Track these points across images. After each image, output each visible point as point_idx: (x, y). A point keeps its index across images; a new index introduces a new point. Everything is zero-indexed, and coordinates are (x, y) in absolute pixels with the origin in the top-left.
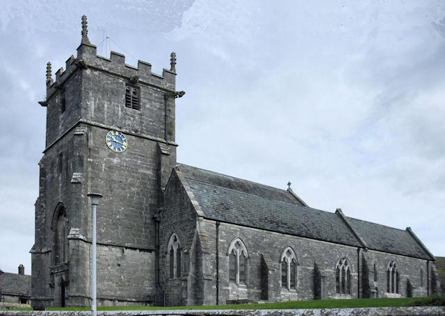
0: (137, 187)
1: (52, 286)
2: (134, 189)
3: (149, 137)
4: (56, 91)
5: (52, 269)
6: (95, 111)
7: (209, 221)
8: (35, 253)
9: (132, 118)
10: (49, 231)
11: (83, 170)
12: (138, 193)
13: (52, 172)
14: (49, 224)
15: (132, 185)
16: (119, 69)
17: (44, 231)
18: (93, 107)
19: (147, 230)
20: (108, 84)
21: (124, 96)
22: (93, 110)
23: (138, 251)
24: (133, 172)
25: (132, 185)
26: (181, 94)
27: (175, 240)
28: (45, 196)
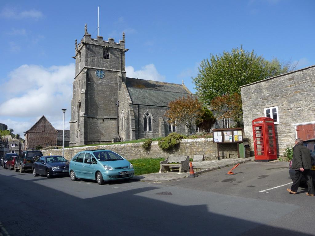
0: (109, 92)
1: (77, 137)
2: (108, 93)
3: (114, 70)
4: (78, 53)
5: (77, 129)
6: (91, 62)
7: (134, 105)
8: (71, 123)
9: (106, 63)
10: (76, 113)
11: (239, 154)
12: (109, 95)
13: (77, 87)
14: (76, 110)
15: (106, 91)
16: (100, 43)
17: (75, 112)
18: (90, 60)
19: (114, 110)
20: (96, 50)
21: (103, 54)
22: (90, 61)
23: (110, 119)
24: (107, 86)
25: (106, 91)
26: (127, 50)
27: (123, 114)
28: (75, 98)
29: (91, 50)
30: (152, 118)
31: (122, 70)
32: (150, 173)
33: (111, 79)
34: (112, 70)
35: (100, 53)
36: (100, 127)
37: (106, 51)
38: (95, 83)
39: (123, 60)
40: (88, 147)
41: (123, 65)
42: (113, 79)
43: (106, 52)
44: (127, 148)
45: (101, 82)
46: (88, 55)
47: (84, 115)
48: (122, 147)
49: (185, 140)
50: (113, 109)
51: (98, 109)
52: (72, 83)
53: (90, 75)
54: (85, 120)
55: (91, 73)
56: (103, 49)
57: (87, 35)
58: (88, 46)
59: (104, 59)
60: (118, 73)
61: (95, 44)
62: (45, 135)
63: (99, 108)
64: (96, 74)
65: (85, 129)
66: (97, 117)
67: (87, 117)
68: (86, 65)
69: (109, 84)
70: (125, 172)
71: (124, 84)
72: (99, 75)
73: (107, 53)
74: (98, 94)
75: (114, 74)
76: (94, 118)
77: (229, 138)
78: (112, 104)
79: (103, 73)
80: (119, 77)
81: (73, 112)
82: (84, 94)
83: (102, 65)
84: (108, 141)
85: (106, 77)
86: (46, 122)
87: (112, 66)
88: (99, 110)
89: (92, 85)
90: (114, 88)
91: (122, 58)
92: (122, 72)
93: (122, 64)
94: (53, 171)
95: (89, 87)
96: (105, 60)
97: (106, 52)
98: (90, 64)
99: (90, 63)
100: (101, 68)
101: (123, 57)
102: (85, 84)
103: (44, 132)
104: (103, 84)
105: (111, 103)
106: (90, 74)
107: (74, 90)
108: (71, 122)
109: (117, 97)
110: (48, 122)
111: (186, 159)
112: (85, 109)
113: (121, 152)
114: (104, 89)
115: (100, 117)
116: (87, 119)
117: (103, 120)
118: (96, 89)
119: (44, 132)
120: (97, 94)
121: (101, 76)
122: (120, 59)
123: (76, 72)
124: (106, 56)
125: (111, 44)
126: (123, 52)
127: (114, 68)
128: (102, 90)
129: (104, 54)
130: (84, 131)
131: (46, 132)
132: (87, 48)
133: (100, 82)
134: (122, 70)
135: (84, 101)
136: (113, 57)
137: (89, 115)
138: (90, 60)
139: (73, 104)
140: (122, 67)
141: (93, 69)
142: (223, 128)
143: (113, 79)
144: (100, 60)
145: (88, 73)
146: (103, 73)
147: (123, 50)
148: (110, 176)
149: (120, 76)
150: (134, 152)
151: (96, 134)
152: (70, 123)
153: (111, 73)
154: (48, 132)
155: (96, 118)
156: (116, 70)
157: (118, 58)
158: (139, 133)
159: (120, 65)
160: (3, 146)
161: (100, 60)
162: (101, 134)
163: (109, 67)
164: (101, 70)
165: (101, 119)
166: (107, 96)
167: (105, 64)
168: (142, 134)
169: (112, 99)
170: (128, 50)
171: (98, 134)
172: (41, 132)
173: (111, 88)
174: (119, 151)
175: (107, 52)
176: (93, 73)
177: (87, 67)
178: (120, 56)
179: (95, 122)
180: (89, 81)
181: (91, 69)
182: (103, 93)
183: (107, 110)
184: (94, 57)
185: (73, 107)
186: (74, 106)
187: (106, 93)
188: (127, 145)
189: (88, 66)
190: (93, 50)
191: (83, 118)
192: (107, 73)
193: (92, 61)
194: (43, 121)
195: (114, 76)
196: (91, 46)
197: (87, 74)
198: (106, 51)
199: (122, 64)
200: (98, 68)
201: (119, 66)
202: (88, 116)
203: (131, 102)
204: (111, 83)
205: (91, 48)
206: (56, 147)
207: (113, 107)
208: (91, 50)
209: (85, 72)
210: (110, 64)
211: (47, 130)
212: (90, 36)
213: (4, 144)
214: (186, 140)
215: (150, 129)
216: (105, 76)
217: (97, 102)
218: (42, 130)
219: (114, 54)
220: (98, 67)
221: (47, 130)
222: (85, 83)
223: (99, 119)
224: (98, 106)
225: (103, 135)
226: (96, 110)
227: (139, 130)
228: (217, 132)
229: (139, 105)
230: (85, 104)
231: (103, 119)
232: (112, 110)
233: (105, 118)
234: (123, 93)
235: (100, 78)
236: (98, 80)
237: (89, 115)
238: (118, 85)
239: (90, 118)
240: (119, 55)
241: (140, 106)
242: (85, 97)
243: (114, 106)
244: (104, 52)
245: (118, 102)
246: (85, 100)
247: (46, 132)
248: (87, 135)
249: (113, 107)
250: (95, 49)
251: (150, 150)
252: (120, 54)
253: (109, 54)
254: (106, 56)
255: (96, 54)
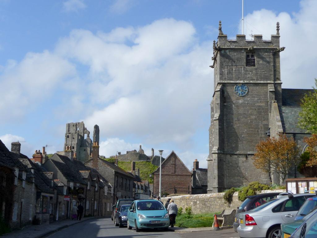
2: (253, 117)
3: (262, 82)
6: (227, 74)
9: (250, 73)
12: (255, 119)
15: (252, 114)
16: (242, 45)
18: (226, 72)
20: (234, 55)
21: (245, 60)
22: (226, 73)
26: (283, 49)
29: (228, 57)
31: (275, 80)
32: (205, 227)
33: (259, 95)
34: (259, 82)
35: (240, 59)
36: (242, 168)
37: (250, 54)
38: (234, 104)
39: (277, 65)
40: (182, 197)
41: (277, 73)
42: (261, 95)
43: (250, 57)
44: (212, 199)
45: (243, 101)
46: (223, 65)
47: (218, 150)
48: (208, 197)
49: (264, 191)
51: (238, 141)
52: (210, 103)
53: (226, 93)
54: (218, 157)
55: (228, 90)
56: (245, 54)
57: (222, 37)
58: (223, 52)
59: (246, 67)
60: (269, 86)
61: (233, 47)
62: (175, 179)
63: (241, 139)
64: (235, 90)
65: (218, 171)
66: (238, 152)
67: (222, 153)
68: (221, 79)
69: (255, 104)
70: (157, 222)
71: (274, 102)
72: (240, 92)
73: (251, 57)
74: (238, 120)
75: (263, 87)
76: (232, 154)
77: (304, 190)
78: (260, 132)
79: (246, 88)
80: (270, 91)
81: (211, 145)
82: (217, 121)
83: (244, 77)
85: (250, 93)
86: (177, 161)
87: (259, 76)
88: (240, 143)
89: (230, 107)
90: (263, 109)
91: (275, 62)
92: (275, 84)
93: (275, 71)
94: (123, 220)
95: (225, 110)
96: (249, 68)
97: (250, 57)
98: (226, 77)
99: (226, 76)
100: (242, 82)
101: (277, 60)
102: (219, 107)
103: (174, 174)
104: (246, 104)
105: (258, 131)
106: (227, 92)
107: (212, 113)
108: (209, 159)
109: (268, 122)
110: (179, 160)
111: (232, 213)
112: (218, 142)
113: (207, 203)
114: (248, 112)
115: (242, 152)
116: (223, 156)
117: (247, 157)
118: (235, 112)
119: (174, 174)
120: (237, 119)
121: (243, 93)
122: (272, 64)
124: (250, 62)
125: (258, 43)
126: (276, 53)
127: (263, 78)
128: (244, 114)
129: (247, 59)
130: (217, 174)
131: (176, 173)
132: (221, 55)
133: (240, 101)
134: (275, 80)
135: (218, 131)
136: (261, 62)
137: (226, 150)
138: (226, 71)
139: (212, 133)
140: (275, 75)
141: (230, 84)
143: (261, 95)
145: (223, 90)
146: (246, 88)
147: (277, 49)
148: (142, 224)
149: (271, 90)
150: (218, 205)
151: (236, 178)
152: (208, 161)
153: (258, 87)
154: (180, 173)
155: (236, 155)
156: (265, 82)
157: (269, 62)
159: (272, 73)
160: (140, 191)
161: (240, 69)
162: (243, 177)
163: (255, 78)
164: (242, 84)
165: (243, 156)
166: (252, 122)
167: (249, 74)
169: (261, 125)
171: (239, 178)
172: (170, 173)
173: (259, 109)
174: (206, 202)
175: (252, 56)
176: (230, 90)
177: (222, 81)
178: (272, 60)
179: (235, 159)
180: (225, 102)
181: (228, 85)
182: (246, 118)
183: (252, 142)
184: (231, 67)
185: (212, 138)
186: (212, 136)
188: (213, 195)
189: (223, 80)
190: (231, 56)
191: (216, 155)
192: (251, 88)
193: (229, 73)
194: (173, 159)
195: (263, 91)
196: (227, 51)
197: (222, 91)
198: (250, 54)
199: (275, 71)
200: (238, 82)
201: (271, 75)
202: (224, 151)
203: (281, 130)
204: (258, 102)
205: (228, 53)
206: (173, 194)
207: (261, 137)
208: (228, 57)
209: (219, 89)
211: (179, 172)
212: (227, 36)
213: (142, 189)
214: (265, 191)
216: (248, 92)
217: (236, 131)
218: (172, 171)
219: (262, 58)
220: (238, 80)
221: (179, 172)
222: (219, 105)
223: (240, 156)
224: (238, 137)
225: (246, 179)
228: (291, 182)
229: (294, 134)
230: (218, 136)
231: (246, 156)
233: (249, 155)
234: (274, 116)
235: (241, 95)
236: (238, 99)
238: (269, 103)
239: (227, 154)
240: (270, 58)
241: (297, 135)
242: (219, 125)
243: (263, 136)
244: (248, 56)
245: (269, 129)
246: (219, 129)
247: (176, 173)
248: (224, 179)
249: (261, 137)
250: (234, 55)
251: (232, 202)
252: (272, 56)
253: (254, 59)
254: (250, 62)
255: (234, 62)
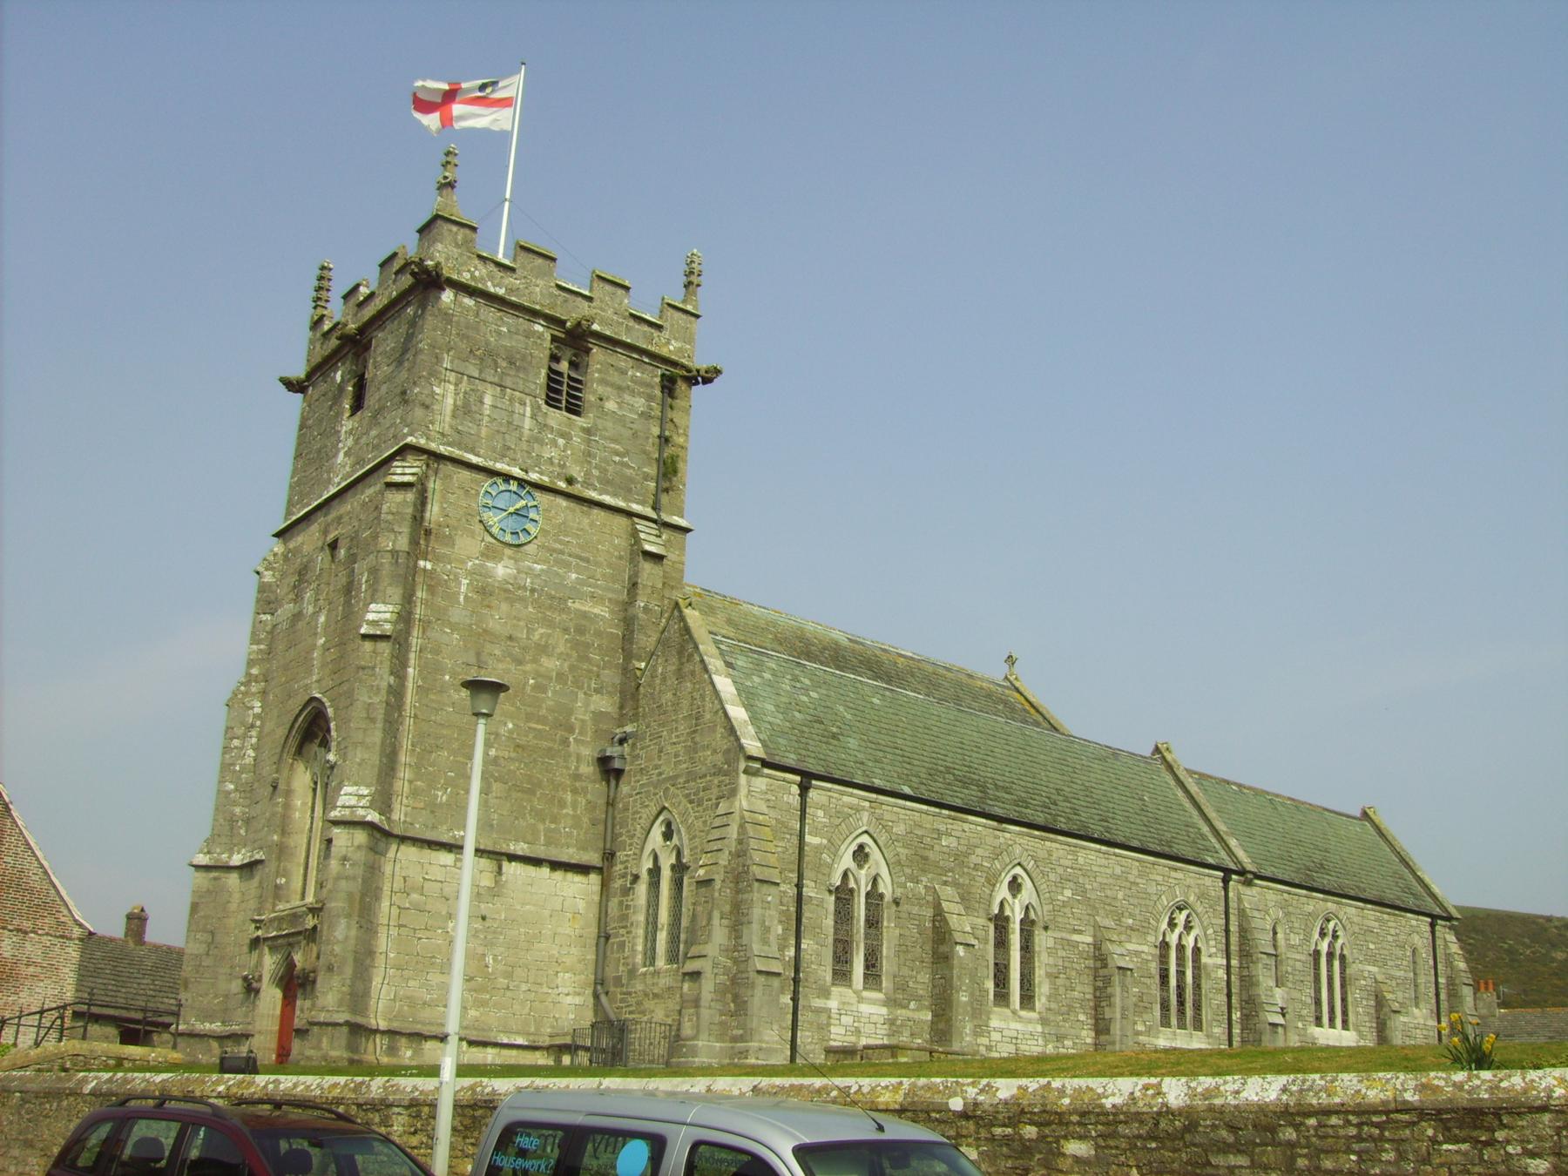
2: (551, 664)
3: (607, 499)
6: (454, 416)
8: (207, 868)
9: (561, 441)
12: (560, 676)
15: (544, 649)
16: (537, 292)
18: (450, 401)
20: (499, 333)
25: (544, 649)
30: (885, 888)
33: (587, 561)
34: (594, 495)
42: (597, 564)
48: (1262, 1109)
50: (575, 791)
78: (573, 747)
84: (520, 1041)
96: (557, 417)
104: (525, 588)
105: (565, 742)
108: (202, 859)
123: (299, 488)
128: (510, 638)
137: (398, 814)
142: (1436, 1042)
143: (597, 564)
144: (517, 407)
152: (198, 867)
158: (795, 999)
161: (517, 407)
168: (818, 1011)
170: (718, 372)
173: (581, 630)
182: (520, 662)
183: (531, 792)
187: (535, 661)
193: (465, 410)
207: (577, 777)
210: (589, 454)
215: (1027, 999)
226: (449, 783)
227: (797, 970)
232: (569, 797)
233: (512, 858)
237: (395, 816)
